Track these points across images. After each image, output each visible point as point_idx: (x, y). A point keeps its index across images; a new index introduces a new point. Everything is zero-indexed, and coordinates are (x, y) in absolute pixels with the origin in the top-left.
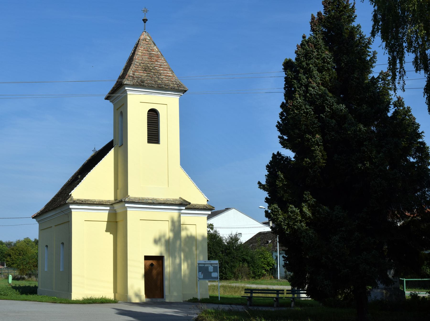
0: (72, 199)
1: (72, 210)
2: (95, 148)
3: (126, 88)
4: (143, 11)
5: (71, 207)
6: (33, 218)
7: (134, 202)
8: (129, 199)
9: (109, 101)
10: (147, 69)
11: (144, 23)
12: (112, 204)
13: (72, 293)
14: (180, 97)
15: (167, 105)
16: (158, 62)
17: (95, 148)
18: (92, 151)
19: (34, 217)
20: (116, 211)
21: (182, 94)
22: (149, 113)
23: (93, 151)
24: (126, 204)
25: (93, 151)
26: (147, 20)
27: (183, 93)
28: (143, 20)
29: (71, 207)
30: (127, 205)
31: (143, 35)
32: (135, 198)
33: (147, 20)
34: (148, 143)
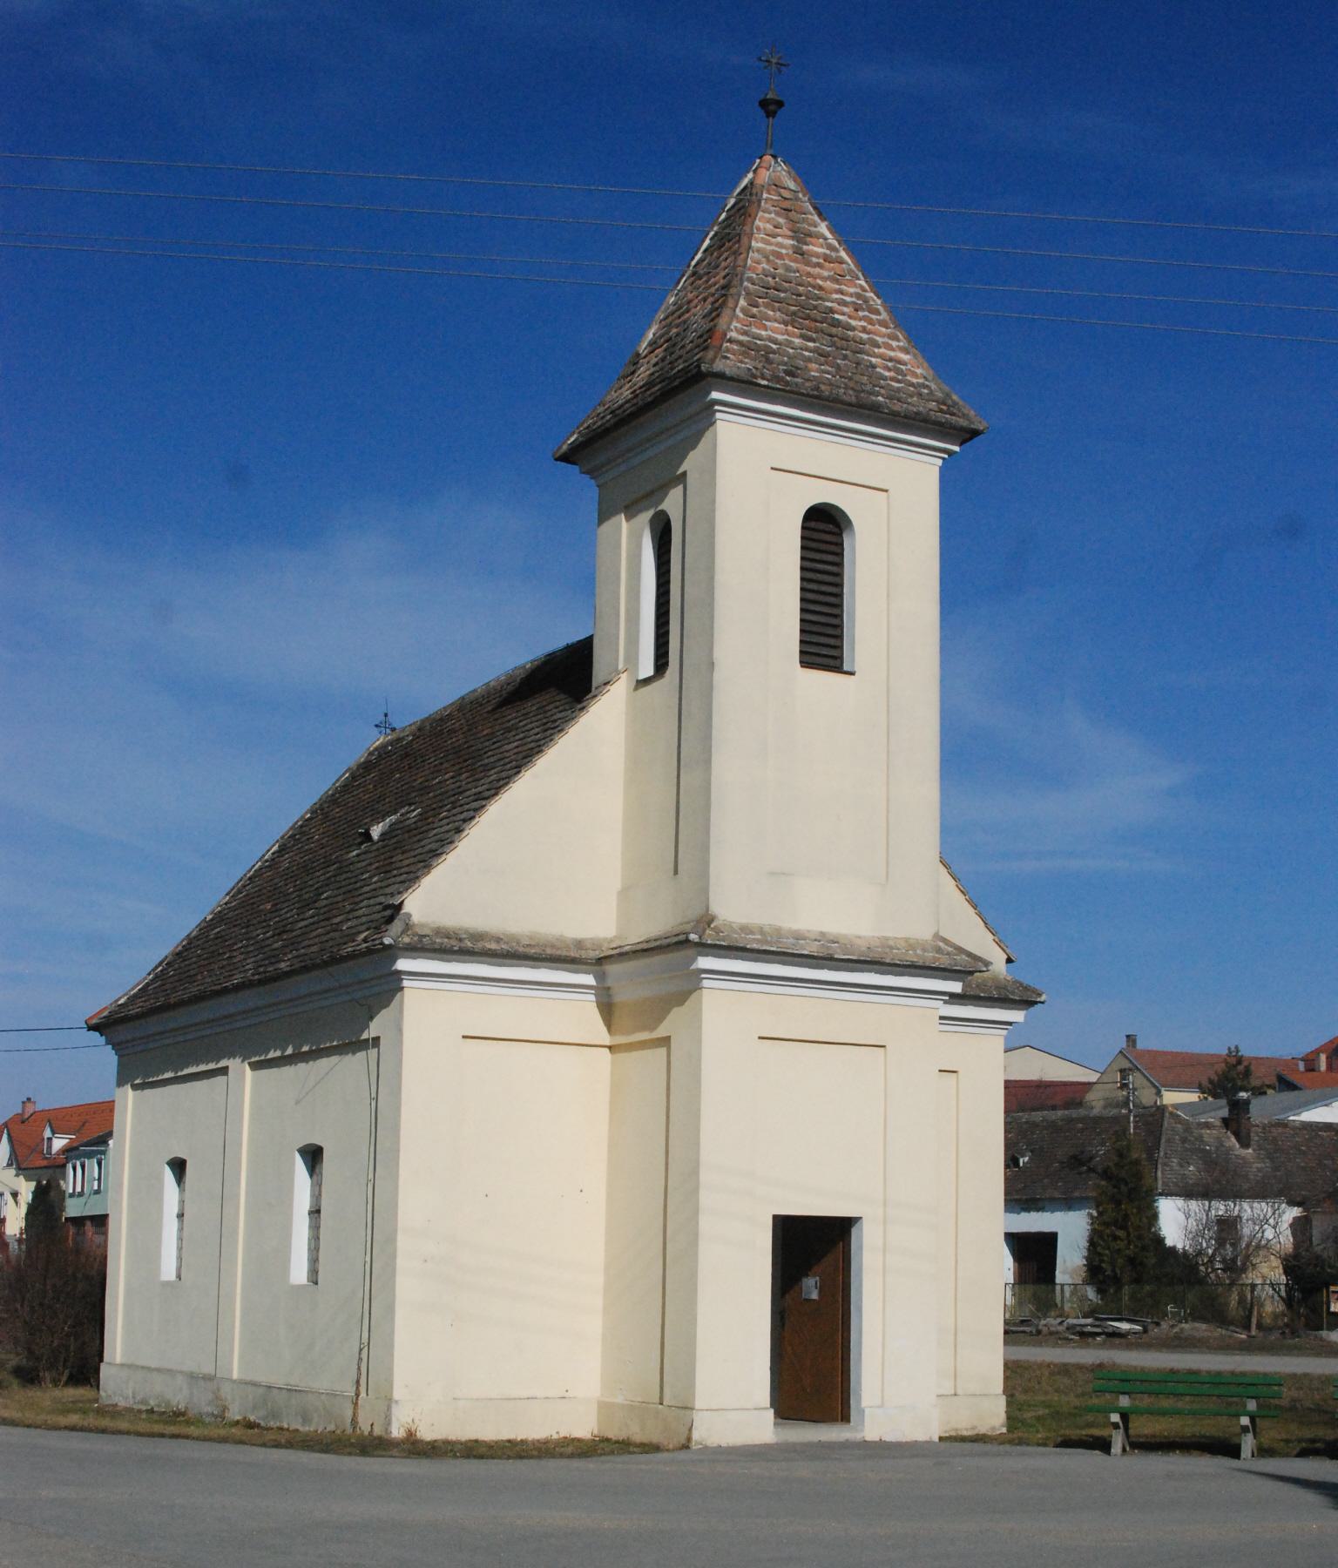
0: (408, 927)
1: (405, 983)
2: (386, 715)
3: (715, 395)
4: (767, 64)
5: (403, 964)
6: (91, 1028)
7: (744, 949)
8: (717, 931)
9: (576, 468)
10: (802, 318)
11: (768, 117)
12: (600, 961)
13: (1005, 1409)
14: (943, 459)
15: (886, 491)
16: (842, 294)
17: (386, 715)
18: (376, 729)
19: (105, 1025)
20: (610, 996)
21: (956, 448)
22: (808, 524)
23: (377, 726)
24: (700, 958)
25: (377, 726)
26: (780, 104)
27: (961, 445)
28: (764, 104)
29: (403, 964)
30: (705, 962)
31: (768, 170)
32: (745, 929)
33: (780, 104)
34: (805, 664)
